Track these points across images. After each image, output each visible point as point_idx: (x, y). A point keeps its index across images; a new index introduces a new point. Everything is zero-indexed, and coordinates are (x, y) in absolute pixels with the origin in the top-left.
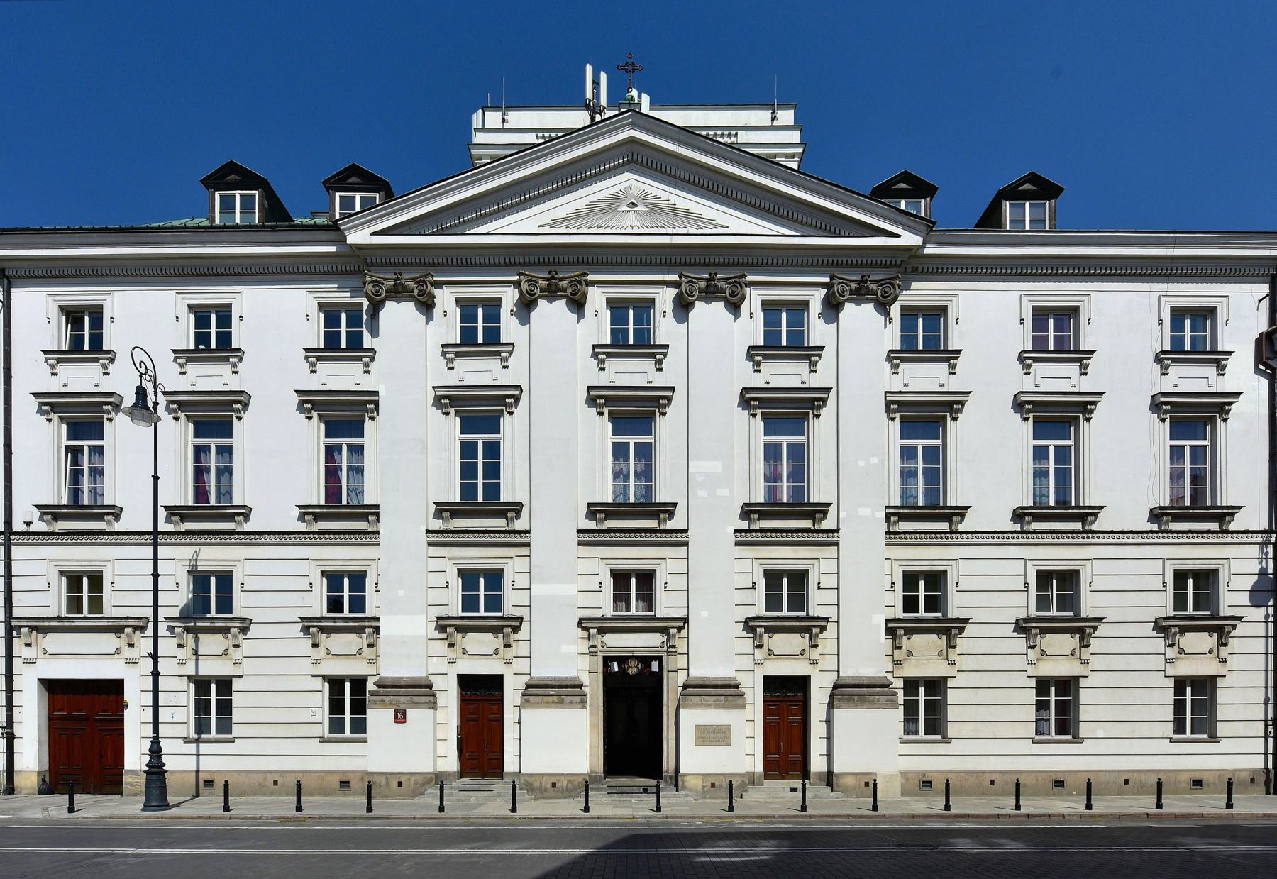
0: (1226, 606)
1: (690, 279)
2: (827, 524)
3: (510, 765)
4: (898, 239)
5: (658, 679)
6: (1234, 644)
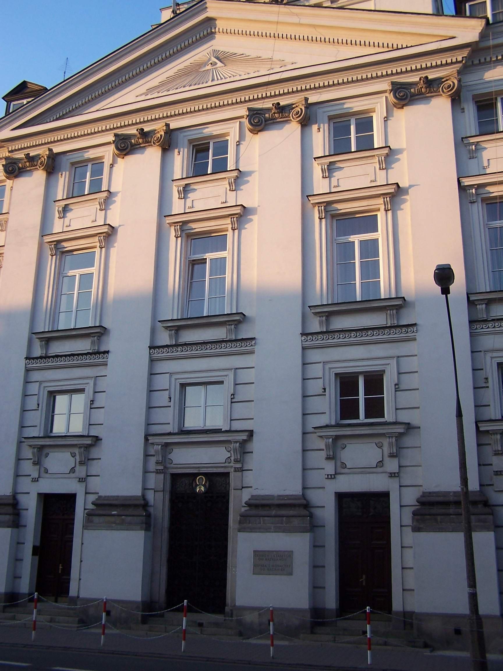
0: (328, 413)
1: (255, 112)
2: (245, 333)
3: (73, 592)
5: (225, 498)
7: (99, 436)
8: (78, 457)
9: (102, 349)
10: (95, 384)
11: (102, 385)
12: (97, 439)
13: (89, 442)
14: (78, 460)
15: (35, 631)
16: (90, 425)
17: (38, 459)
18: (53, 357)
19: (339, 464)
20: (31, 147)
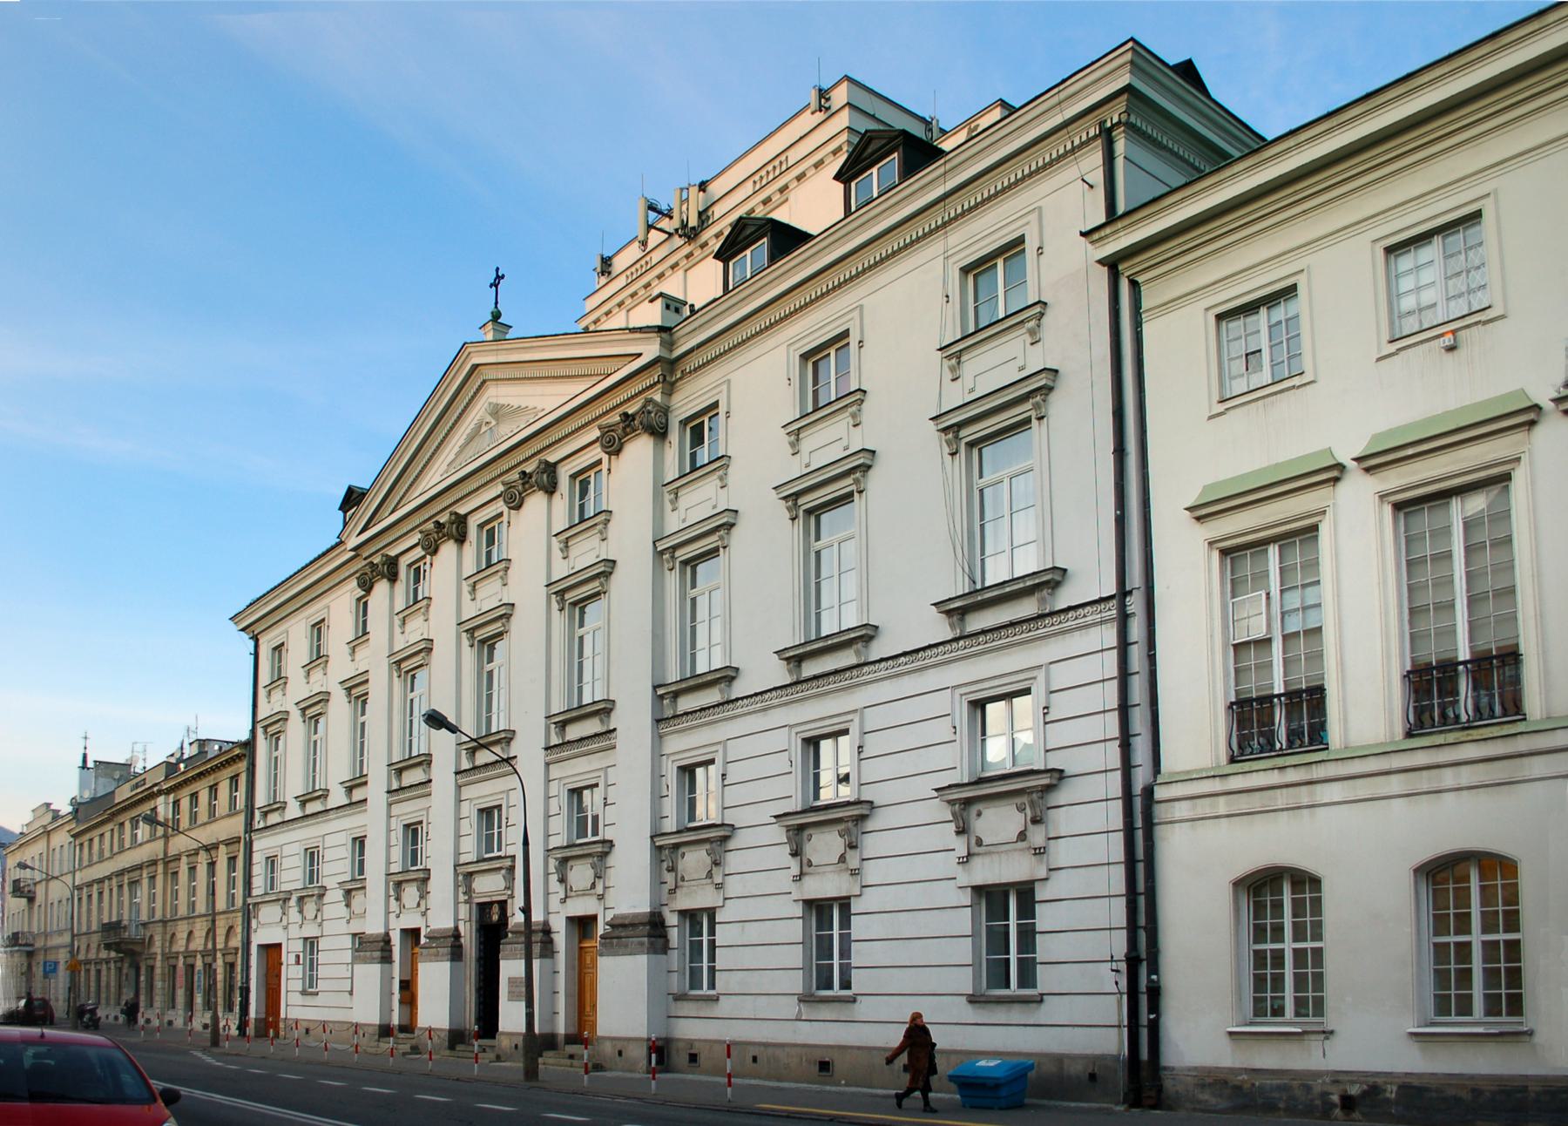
4: (1004, 99)
6: (1062, 821)
8: (1028, 811)
9: (611, 728)
13: (1046, 781)
14: (1029, 818)
15: (521, 1076)
17: (964, 823)
18: (682, 715)
19: (679, 876)
20: (625, 402)
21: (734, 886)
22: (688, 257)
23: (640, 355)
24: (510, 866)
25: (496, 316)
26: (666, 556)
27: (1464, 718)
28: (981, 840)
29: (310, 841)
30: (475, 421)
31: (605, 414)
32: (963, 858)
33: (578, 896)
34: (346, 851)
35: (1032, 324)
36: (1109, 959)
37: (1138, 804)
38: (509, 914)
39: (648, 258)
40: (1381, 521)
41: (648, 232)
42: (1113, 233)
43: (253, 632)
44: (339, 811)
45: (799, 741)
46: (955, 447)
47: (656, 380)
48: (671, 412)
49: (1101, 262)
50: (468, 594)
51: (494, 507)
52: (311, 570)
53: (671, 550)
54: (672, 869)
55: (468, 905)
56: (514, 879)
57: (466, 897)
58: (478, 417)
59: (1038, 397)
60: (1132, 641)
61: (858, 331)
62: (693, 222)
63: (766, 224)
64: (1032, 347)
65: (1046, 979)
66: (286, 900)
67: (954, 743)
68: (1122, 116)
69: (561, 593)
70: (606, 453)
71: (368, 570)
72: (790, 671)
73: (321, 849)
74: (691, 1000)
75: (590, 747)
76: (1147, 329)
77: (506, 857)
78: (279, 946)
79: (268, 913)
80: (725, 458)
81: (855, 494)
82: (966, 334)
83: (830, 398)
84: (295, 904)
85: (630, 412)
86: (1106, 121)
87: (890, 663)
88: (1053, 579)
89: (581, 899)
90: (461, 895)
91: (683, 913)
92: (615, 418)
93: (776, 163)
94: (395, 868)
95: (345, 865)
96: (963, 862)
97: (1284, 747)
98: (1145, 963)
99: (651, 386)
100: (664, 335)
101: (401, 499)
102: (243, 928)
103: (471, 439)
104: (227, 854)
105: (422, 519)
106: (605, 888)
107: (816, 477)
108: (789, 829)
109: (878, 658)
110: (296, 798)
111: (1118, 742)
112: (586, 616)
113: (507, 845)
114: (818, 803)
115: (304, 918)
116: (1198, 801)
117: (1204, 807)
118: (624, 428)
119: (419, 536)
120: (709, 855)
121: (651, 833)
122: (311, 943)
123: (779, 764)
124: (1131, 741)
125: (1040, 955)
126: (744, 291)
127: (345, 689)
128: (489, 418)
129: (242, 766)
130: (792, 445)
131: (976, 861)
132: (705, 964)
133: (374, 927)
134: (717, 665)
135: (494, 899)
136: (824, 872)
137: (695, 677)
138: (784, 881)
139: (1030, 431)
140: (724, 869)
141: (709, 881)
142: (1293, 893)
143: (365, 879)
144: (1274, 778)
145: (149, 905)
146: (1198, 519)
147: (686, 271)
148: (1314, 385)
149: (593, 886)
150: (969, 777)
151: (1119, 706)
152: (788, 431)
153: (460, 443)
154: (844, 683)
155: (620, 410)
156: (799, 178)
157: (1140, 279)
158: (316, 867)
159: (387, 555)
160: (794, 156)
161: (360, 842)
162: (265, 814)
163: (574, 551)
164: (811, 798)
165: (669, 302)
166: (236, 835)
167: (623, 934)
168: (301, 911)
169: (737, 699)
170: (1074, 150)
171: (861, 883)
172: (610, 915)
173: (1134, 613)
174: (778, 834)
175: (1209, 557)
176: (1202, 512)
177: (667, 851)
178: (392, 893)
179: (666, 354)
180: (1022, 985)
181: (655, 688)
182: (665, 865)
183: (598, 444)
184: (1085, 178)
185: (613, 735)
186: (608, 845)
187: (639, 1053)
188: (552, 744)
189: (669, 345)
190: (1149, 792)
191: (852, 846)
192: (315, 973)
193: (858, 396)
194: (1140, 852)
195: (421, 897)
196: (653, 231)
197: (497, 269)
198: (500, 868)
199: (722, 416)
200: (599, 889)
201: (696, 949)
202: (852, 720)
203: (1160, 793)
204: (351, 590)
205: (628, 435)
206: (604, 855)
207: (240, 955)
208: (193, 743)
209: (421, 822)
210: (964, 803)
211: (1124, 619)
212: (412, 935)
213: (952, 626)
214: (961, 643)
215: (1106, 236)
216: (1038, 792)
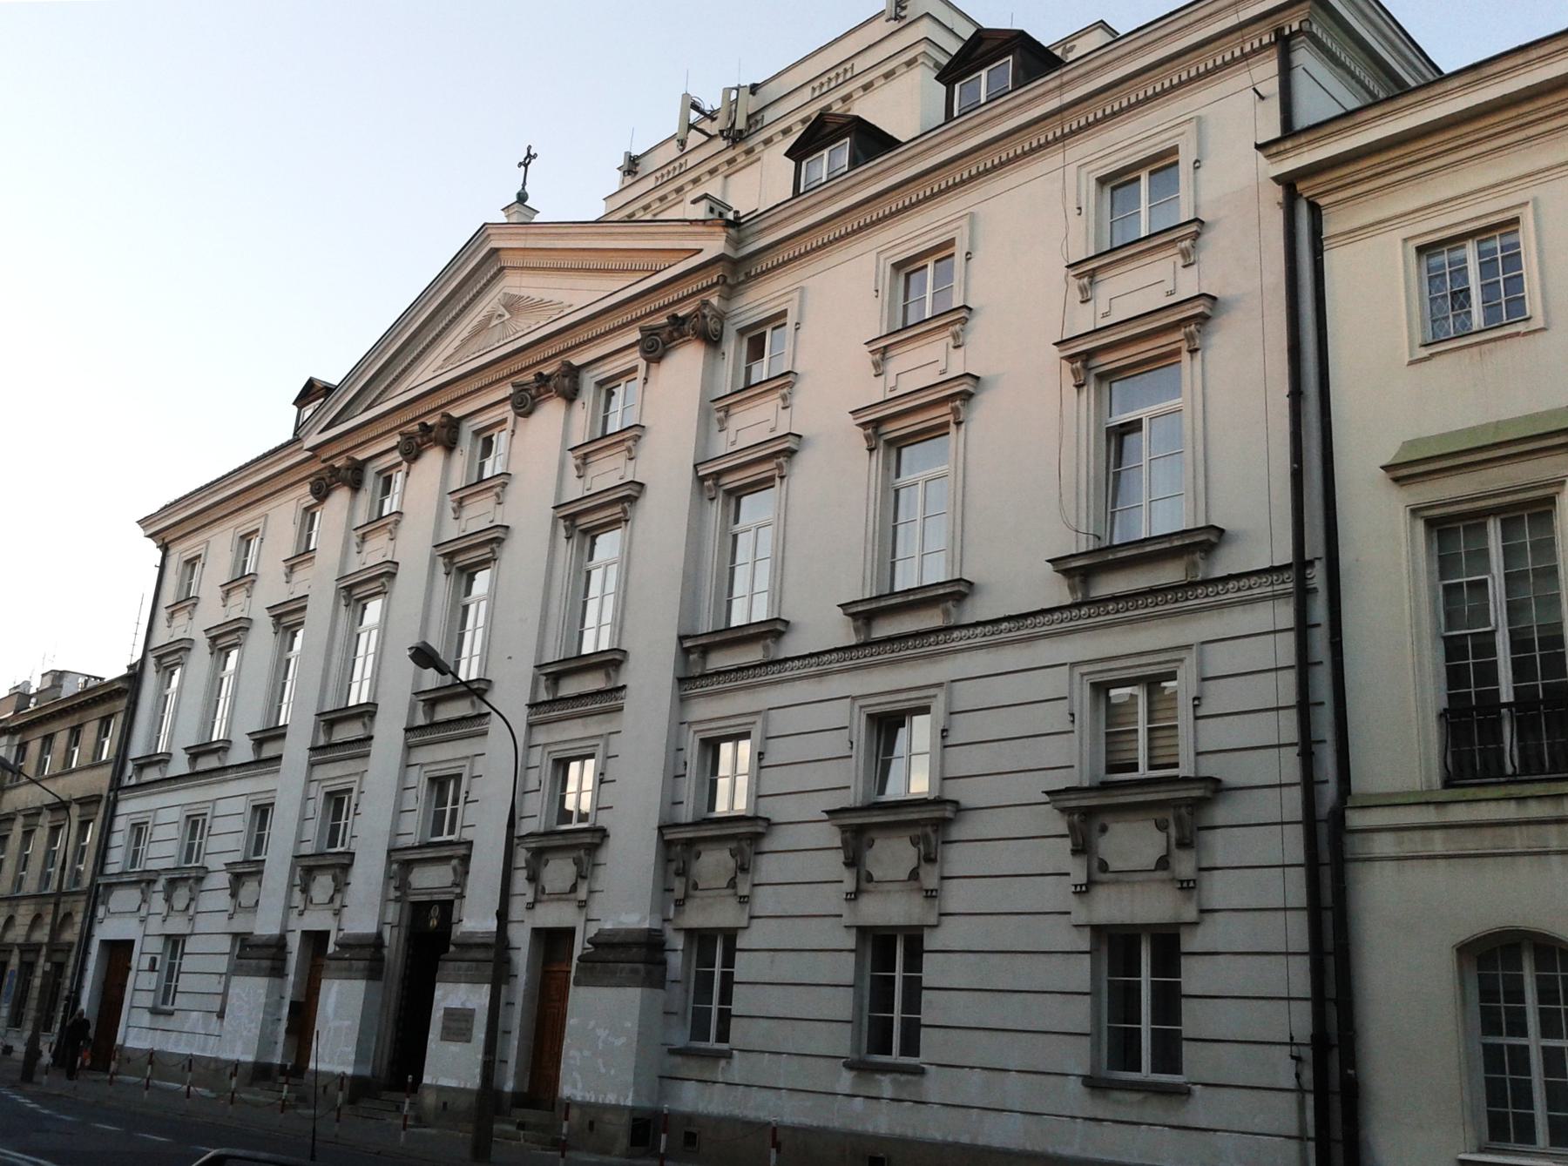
6: (1221, 847)
7: (1223, 779)
8: (1173, 831)
9: (620, 684)
10: (1201, 664)
11: (616, 745)
12: (602, 833)
13: (1197, 793)
14: (1173, 841)
16: (1198, 754)
19: (691, 882)
21: (765, 901)
22: (731, 162)
23: (700, 251)
24: (464, 855)
25: (522, 198)
26: (709, 483)
27: (1509, 769)
28: (1106, 863)
29: (195, 806)
30: (484, 313)
31: (651, 313)
32: (1081, 886)
33: (552, 900)
34: (240, 824)
35: (1187, 243)
36: (1288, 1041)
37: (1323, 831)
38: (455, 918)
39: (682, 161)
40: (1413, 540)
41: (688, 132)
42: (1295, 148)
43: (163, 539)
44: (240, 770)
45: (864, 717)
46: (1082, 378)
47: (715, 280)
48: (728, 319)
49: (1277, 179)
50: (451, 511)
51: (500, 411)
52: (290, 451)
53: (1084, 357)
54: (682, 872)
55: (399, 905)
56: (467, 873)
57: (398, 894)
58: (488, 309)
59: (1193, 326)
60: (1313, 623)
61: (1193, 145)
62: (741, 124)
63: (849, 123)
64: (1083, 305)
65: (1196, 1062)
66: (151, 882)
67: (1071, 735)
68: (1303, 24)
69: (450, 556)
70: (645, 359)
71: (326, 474)
72: (857, 630)
73: (208, 818)
74: (693, 1055)
75: (589, 707)
76: (1331, 259)
77: (458, 843)
78: (131, 943)
79: (125, 899)
80: (791, 375)
81: (952, 424)
82: (737, 389)
83: (762, 376)
84: (161, 889)
85: (680, 315)
86: (1283, 28)
87: (989, 628)
88: (1208, 540)
89: (555, 904)
90: (392, 889)
91: (690, 933)
92: (529, 377)
93: (840, 70)
94: (307, 849)
95: (239, 840)
96: (851, 899)
97: (1518, 772)
98: (1336, 1052)
99: (708, 288)
100: (731, 231)
101: (381, 394)
102: (85, 918)
103: (476, 333)
104: (80, 816)
105: (404, 419)
106: (591, 892)
107: (906, 402)
108: (844, 828)
109: (973, 621)
110: (185, 749)
111: (1296, 750)
112: (596, 547)
113: (463, 827)
114: (884, 799)
115: (171, 908)
116: (1407, 835)
117: (1413, 843)
118: (538, 388)
119: (398, 438)
120: (733, 856)
121: (660, 818)
122: (175, 942)
123: (835, 744)
124: (1313, 749)
125: (1188, 1027)
126: (1180, 20)
127: (273, 616)
128: (502, 310)
129: (122, 704)
130: (876, 365)
131: (1100, 893)
132: (715, 1006)
133: (265, 925)
134: (604, 646)
135: (436, 897)
136: (889, 891)
137: (893, 594)
138: (832, 899)
139: (946, 437)
140: (149, 907)
141: (730, 891)
142: (1537, 969)
143: (264, 861)
144: (1509, 811)
145: (17, 872)
146: (1396, 480)
147: (726, 177)
148: (1545, 333)
149: (574, 888)
150: (1090, 779)
151: (1298, 702)
152: (1077, 272)
153: (461, 337)
154: (997, 637)
155: (670, 311)
156: (887, 76)
157: (1322, 202)
158: (197, 841)
159: (353, 458)
160: (860, 64)
161: (262, 812)
162: (141, 767)
163: (468, 512)
164: (705, 809)
165: (714, 206)
166: (97, 793)
167: (611, 957)
168: (168, 899)
169: (786, 660)
170: (1245, 56)
171: (940, 909)
172: (593, 930)
173: (1315, 588)
174: (830, 835)
175: (1412, 528)
176: (1401, 473)
177: (679, 847)
178: (298, 881)
179: (730, 253)
180: (903, 1053)
181: (681, 638)
182: (673, 866)
183: (637, 348)
184: (1257, 87)
185: (487, 719)
186: (599, 835)
187: (620, 1130)
188: (540, 700)
189: (737, 243)
190: (1338, 816)
191: (929, 859)
192: (173, 984)
193: (963, 314)
194: (1327, 898)
195: (337, 890)
196: (693, 131)
197: (529, 148)
198: (449, 858)
199: (959, 258)
200: (582, 893)
201: (704, 982)
202: (935, 696)
203: (1355, 819)
204: (303, 495)
205: (674, 340)
206: (593, 849)
207: (74, 953)
208: (47, 674)
209: (350, 790)
210: (1084, 814)
211: (1303, 596)
212: (315, 940)
213: (1072, 589)
214: (1084, 611)
215: (1286, 151)
216: (747, 839)
